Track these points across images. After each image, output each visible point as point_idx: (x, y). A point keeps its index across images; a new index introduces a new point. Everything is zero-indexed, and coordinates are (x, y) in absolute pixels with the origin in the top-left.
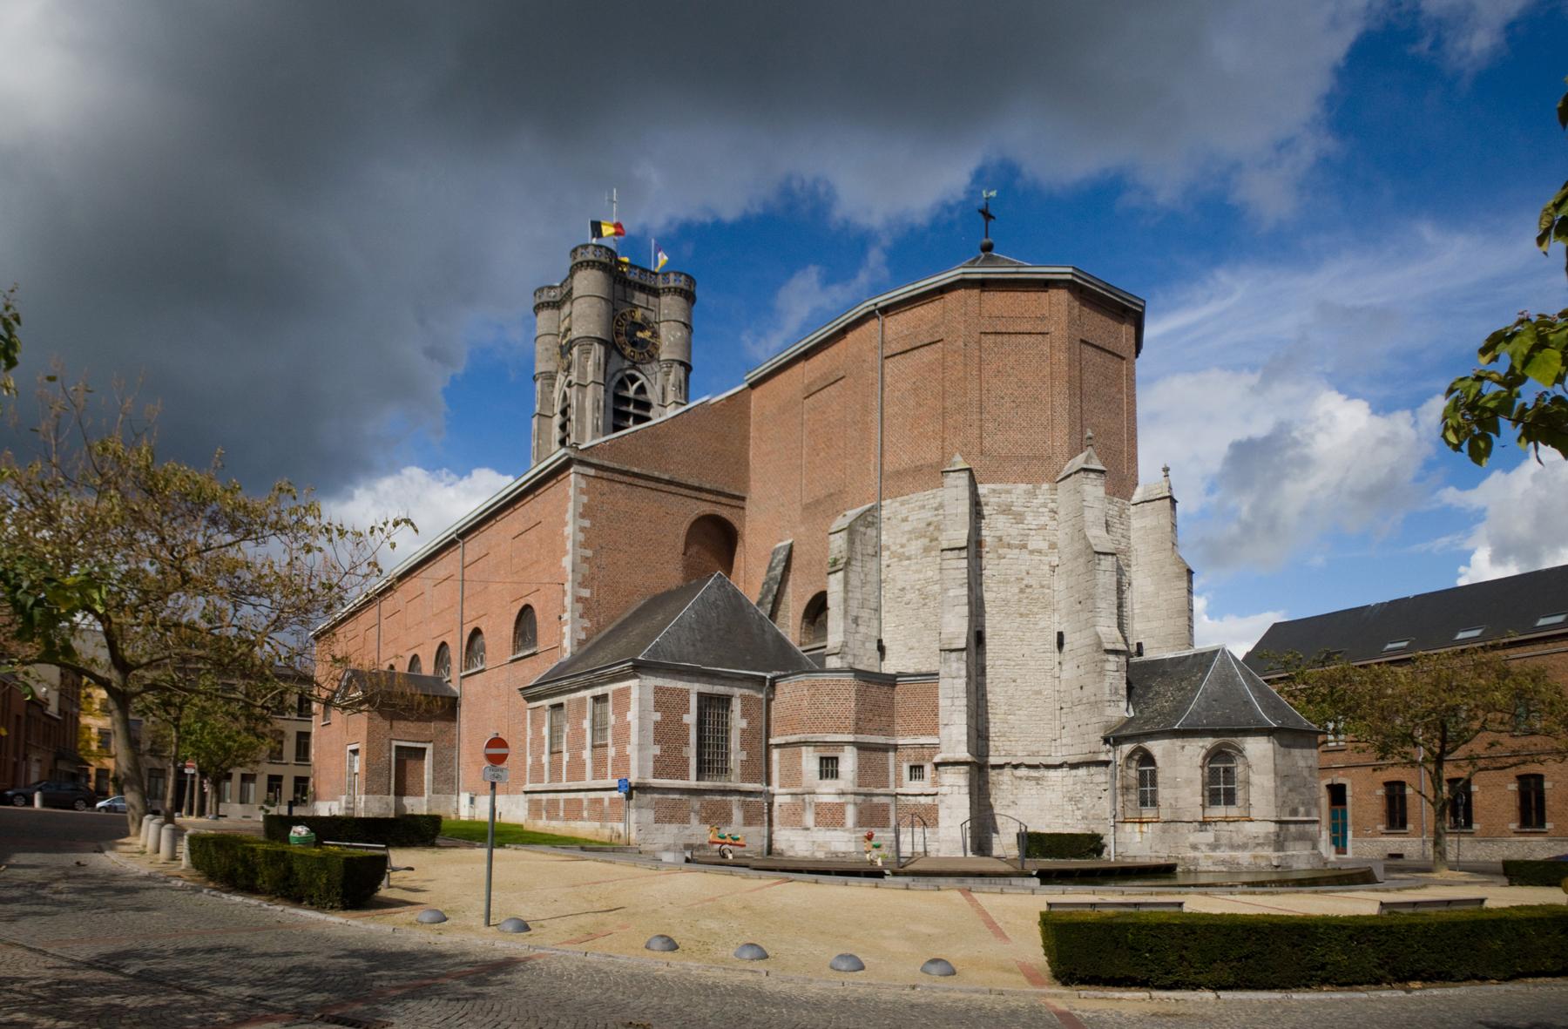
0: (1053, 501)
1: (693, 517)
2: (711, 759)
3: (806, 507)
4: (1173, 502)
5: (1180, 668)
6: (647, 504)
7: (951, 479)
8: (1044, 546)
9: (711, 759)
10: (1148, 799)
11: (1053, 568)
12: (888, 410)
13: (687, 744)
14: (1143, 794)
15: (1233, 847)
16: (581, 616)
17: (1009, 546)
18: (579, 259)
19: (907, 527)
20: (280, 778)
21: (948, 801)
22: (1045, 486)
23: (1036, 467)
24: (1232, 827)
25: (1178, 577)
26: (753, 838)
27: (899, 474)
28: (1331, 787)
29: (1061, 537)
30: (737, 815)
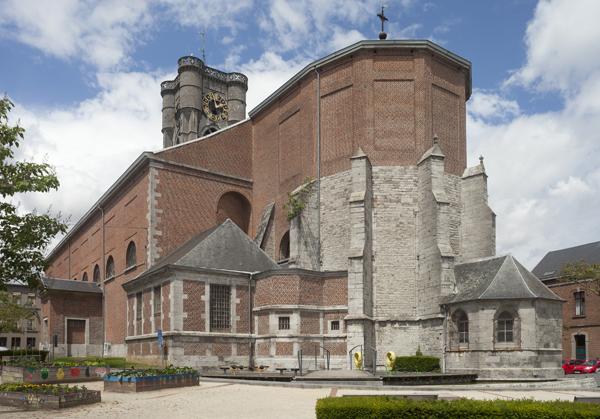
0: (416, 176)
1: (221, 194)
2: (220, 320)
3: (282, 185)
4: (485, 177)
5: (485, 267)
6: (194, 184)
7: (355, 163)
8: (410, 201)
9: (220, 320)
10: (464, 339)
11: (415, 214)
12: (324, 127)
13: (204, 312)
14: (462, 335)
15: (510, 365)
16: (157, 246)
17: (391, 201)
18: (183, 65)
19: (333, 192)
20: (19, 339)
21: (352, 340)
22: (411, 167)
23: (404, 156)
24: (510, 354)
25: (487, 218)
26: (244, 361)
27: (329, 163)
28: (576, 336)
29: (420, 196)
30: (234, 350)
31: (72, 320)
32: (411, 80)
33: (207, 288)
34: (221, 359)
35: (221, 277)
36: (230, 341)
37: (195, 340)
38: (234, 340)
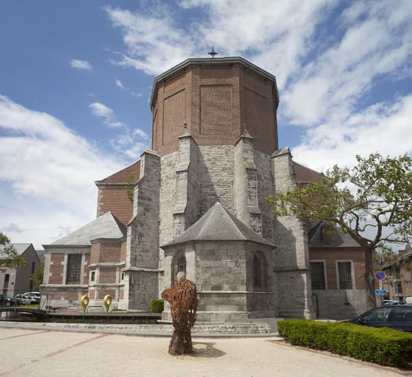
13: (62, 272)
31: (323, 267)
32: (183, 90)
33: (66, 257)
34: (71, 302)
35: (75, 249)
36: (78, 290)
37: (54, 290)
38: (81, 290)
